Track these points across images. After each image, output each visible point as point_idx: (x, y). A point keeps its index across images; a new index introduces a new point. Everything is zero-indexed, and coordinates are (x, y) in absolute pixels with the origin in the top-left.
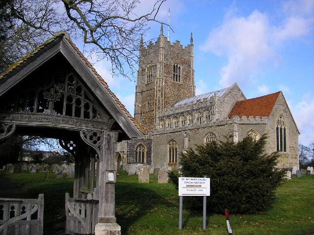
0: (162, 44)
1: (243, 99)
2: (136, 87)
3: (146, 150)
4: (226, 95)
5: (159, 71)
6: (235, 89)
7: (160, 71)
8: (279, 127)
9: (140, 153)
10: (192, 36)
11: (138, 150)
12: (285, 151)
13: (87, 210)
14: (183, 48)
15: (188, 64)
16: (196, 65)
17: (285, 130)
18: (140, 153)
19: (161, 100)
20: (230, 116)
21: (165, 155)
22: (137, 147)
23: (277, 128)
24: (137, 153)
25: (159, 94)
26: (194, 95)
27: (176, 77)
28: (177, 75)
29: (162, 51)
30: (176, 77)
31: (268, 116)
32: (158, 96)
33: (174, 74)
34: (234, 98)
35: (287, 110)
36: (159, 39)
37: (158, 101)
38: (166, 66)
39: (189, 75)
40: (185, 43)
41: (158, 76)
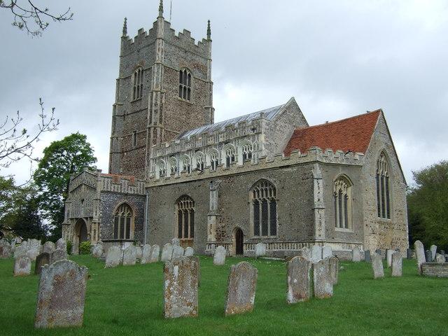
0: (161, 32)
1: (302, 127)
2: (115, 106)
3: (134, 215)
4: (278, 118)
5: (157, 79)
6: (292, 107)
7: (157, 79)
9: (122, 219)
10: (209, 25)
11: (120, 214)
12: (389, 217)
13: (197, 182)
14: (196, 43)
15: (205, 70)
16: (215, 75)
18: (122, 219)
19: (159, 129)
20: (288, 152)
21: (288, 173)
22: (118, 210)
24: (117, 219)
25: (155, 118)
26: (212, 123)
27: (185, 92)
28: (185, 88)
29: (160, 45)
30: (185, 92)
31: (363, 150)
32: (153, 121)
33: (181, 87)
34: (291, 123)
35: (389, 144)
36: (156, 24)
37: (152, 131)
38: (167, 70)
39: (207, 86)
40: (198, 36)
41: (154, 87)
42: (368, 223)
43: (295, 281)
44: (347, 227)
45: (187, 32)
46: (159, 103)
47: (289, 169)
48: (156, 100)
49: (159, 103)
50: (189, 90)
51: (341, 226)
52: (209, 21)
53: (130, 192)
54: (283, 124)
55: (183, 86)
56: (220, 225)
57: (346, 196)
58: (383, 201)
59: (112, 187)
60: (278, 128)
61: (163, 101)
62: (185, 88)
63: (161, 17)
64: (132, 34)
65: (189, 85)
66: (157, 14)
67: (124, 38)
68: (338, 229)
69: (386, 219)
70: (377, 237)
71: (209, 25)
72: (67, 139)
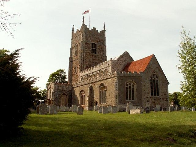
8: (153, 79)
10: (104, 24)
12: (158, 95)
17: (157, 81)
23: (151, 80)
27: (94, 51)
28: (94, 49)
33: (92, 49)
40: (99, 29)
42: (144, 98)
43: (42, 109)
44: (133, 99)
45: (95, 28)
46: (82, 56)
47: (109, 79)
48: (82, 55)
49: (82, 56)
50: (96, 50)
51: (130, 99)
52: (104, 23)
53: (66, 89)
54: (121, 62)
55: (93, 49)
56: (91, 100)
57: (133, 89)
58: (155, 89)
59: (59, 88)
60: (119, 63)
61: (84, 55)
62: (94, 49)
63: (83, 24)
64: (75, 31)
65: (96, 48)
66: (82, 23)
67: (73, 32)
68: (127, 100)
69: (156, 96)
70: (150, 103)
71: (104, 24)
72: (57, 71)
